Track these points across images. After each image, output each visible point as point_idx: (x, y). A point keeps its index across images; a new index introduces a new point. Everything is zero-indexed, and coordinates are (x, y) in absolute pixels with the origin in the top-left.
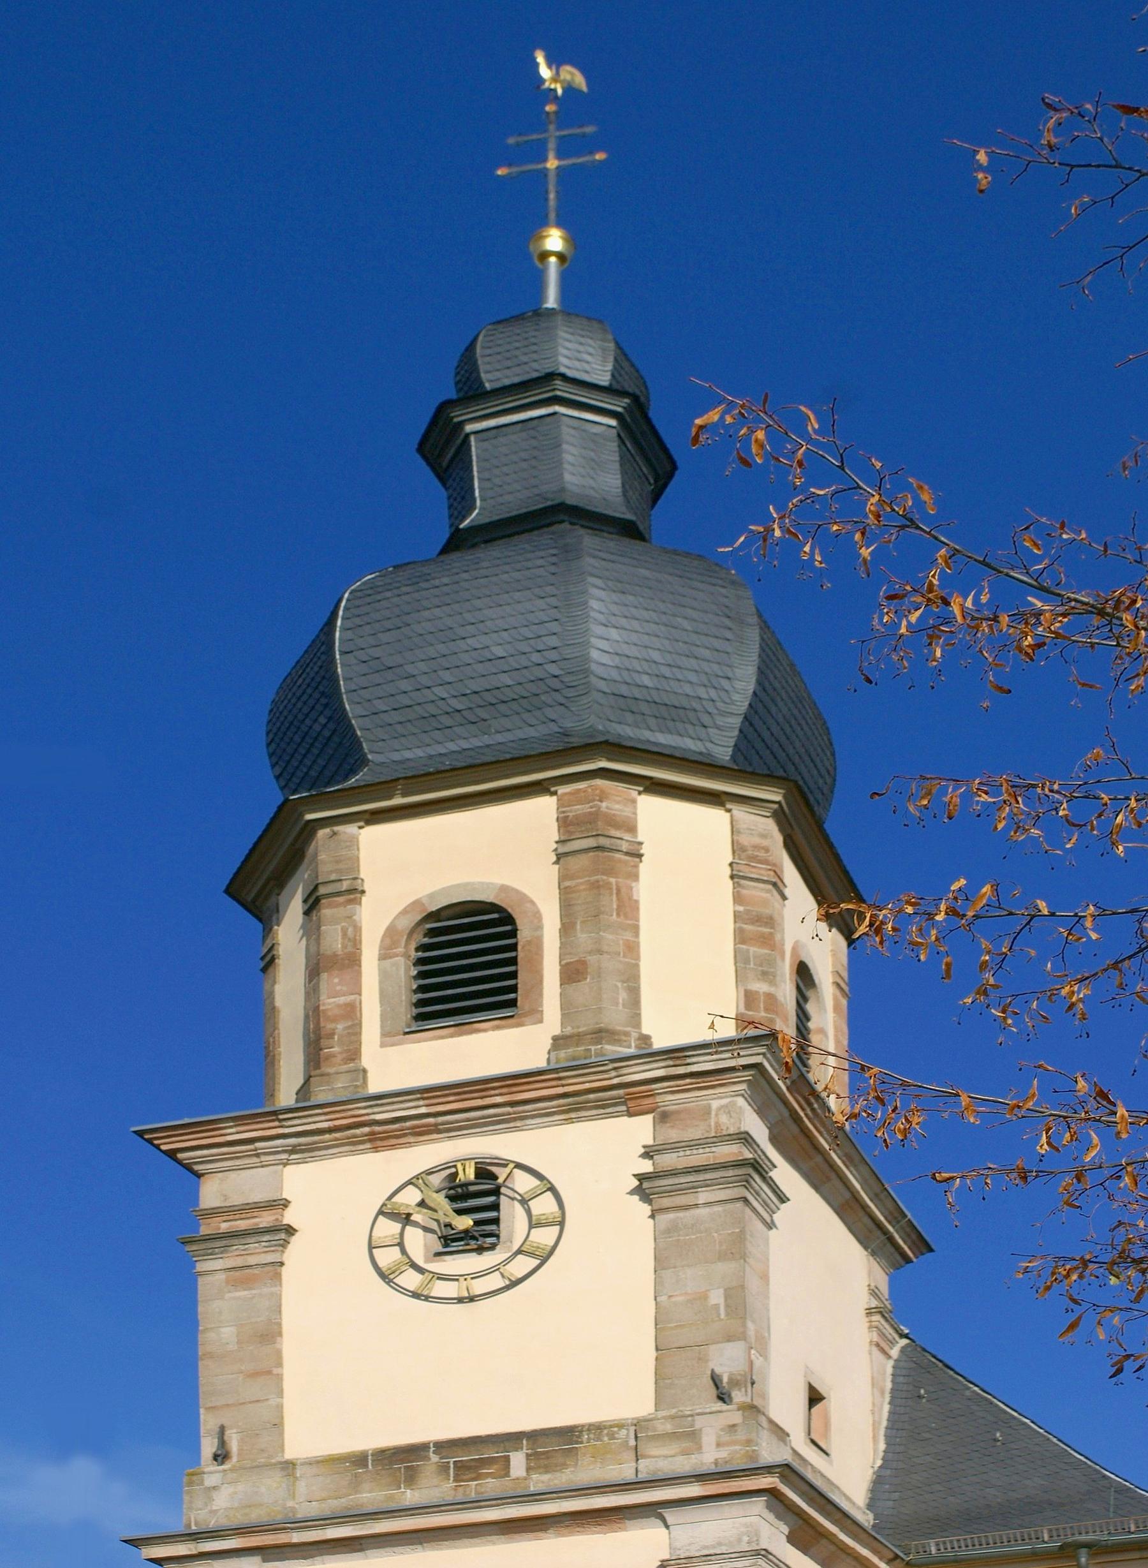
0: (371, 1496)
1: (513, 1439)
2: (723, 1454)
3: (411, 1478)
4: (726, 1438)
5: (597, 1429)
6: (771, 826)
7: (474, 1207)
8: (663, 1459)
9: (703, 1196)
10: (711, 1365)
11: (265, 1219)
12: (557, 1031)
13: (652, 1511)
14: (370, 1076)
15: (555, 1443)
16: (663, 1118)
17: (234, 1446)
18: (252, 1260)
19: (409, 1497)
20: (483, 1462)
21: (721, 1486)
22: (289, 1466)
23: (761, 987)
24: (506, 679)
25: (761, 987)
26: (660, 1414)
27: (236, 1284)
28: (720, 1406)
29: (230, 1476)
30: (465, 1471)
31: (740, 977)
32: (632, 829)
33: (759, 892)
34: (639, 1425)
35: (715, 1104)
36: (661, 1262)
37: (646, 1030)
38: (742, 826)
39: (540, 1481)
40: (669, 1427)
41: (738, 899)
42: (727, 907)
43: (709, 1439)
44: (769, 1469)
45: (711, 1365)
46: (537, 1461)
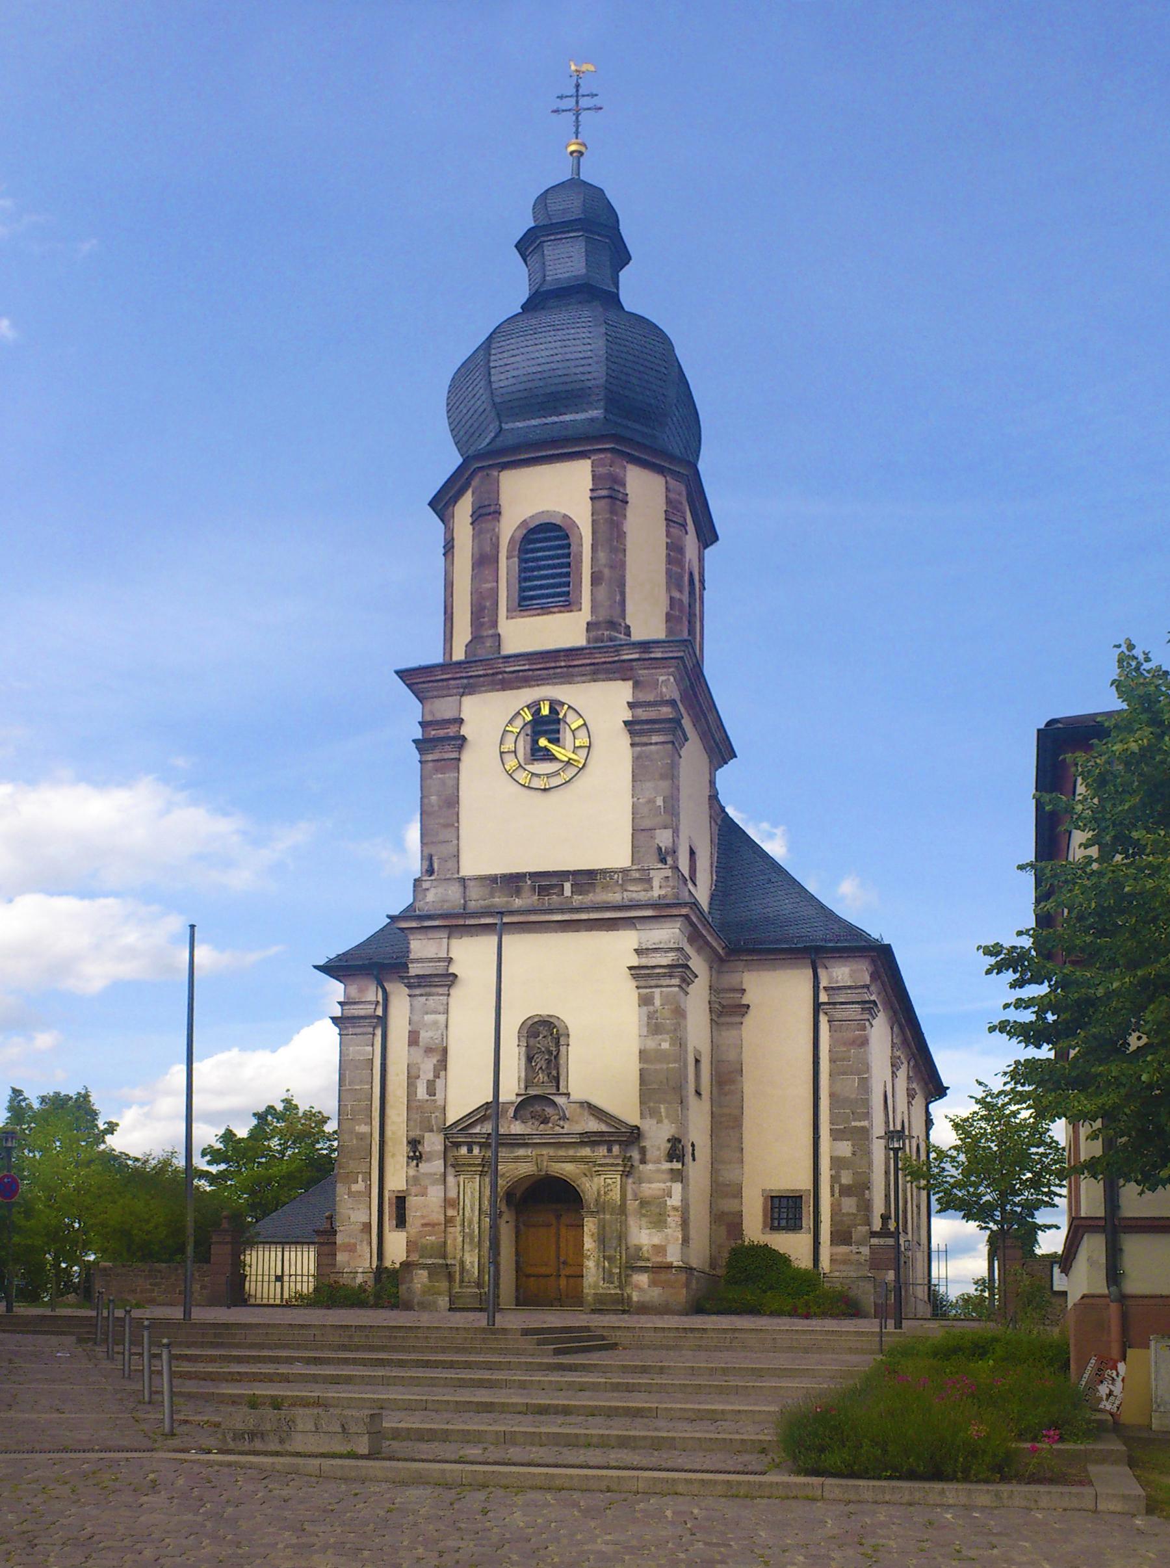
0: (499, 900)
1: (564, 875)
2: (663, 892)
3: (518, 892)
4: (664, 884)
5: (604, 872)
6: (683, 488)
7: (545, 726)
8: (636, 893)
9: (655, 739)
10: (657, 841)
11: (451, 731)
12: (589, 619)
13: (630, 923)
14: (986, 1238)
15: (586, 879)
16: (637, 684)
17: (436, 866)
18: (446, 756)
19: (518, 903)
20: (552, 886)
21: (661, 911)
22: (463, 881)
23: (677, 595)
24: (559, 365)
25: (677, 595)
26: (635, 867)
27: (437, 770)
28: (660, 866)
29: (435, 883)
30: (543, 890)
31: (668, 589)
32: (624, 485)
33: (675, 531)
34: (625, 871)
35: (661, 678)
36: (635, 778)
37: (628, 623)
38: (671, 487)
39: (578, 899)
40: (637, 875)
41: (668, 535)
42: (663, 540)
43: (656, 883)
44: (685, 904)
45: (657, 841)
46: (578, 888)
